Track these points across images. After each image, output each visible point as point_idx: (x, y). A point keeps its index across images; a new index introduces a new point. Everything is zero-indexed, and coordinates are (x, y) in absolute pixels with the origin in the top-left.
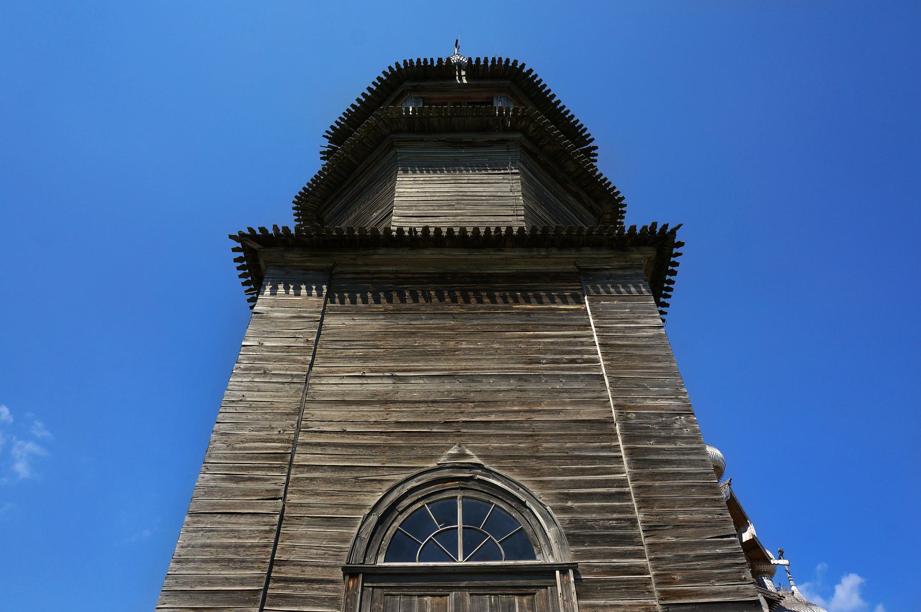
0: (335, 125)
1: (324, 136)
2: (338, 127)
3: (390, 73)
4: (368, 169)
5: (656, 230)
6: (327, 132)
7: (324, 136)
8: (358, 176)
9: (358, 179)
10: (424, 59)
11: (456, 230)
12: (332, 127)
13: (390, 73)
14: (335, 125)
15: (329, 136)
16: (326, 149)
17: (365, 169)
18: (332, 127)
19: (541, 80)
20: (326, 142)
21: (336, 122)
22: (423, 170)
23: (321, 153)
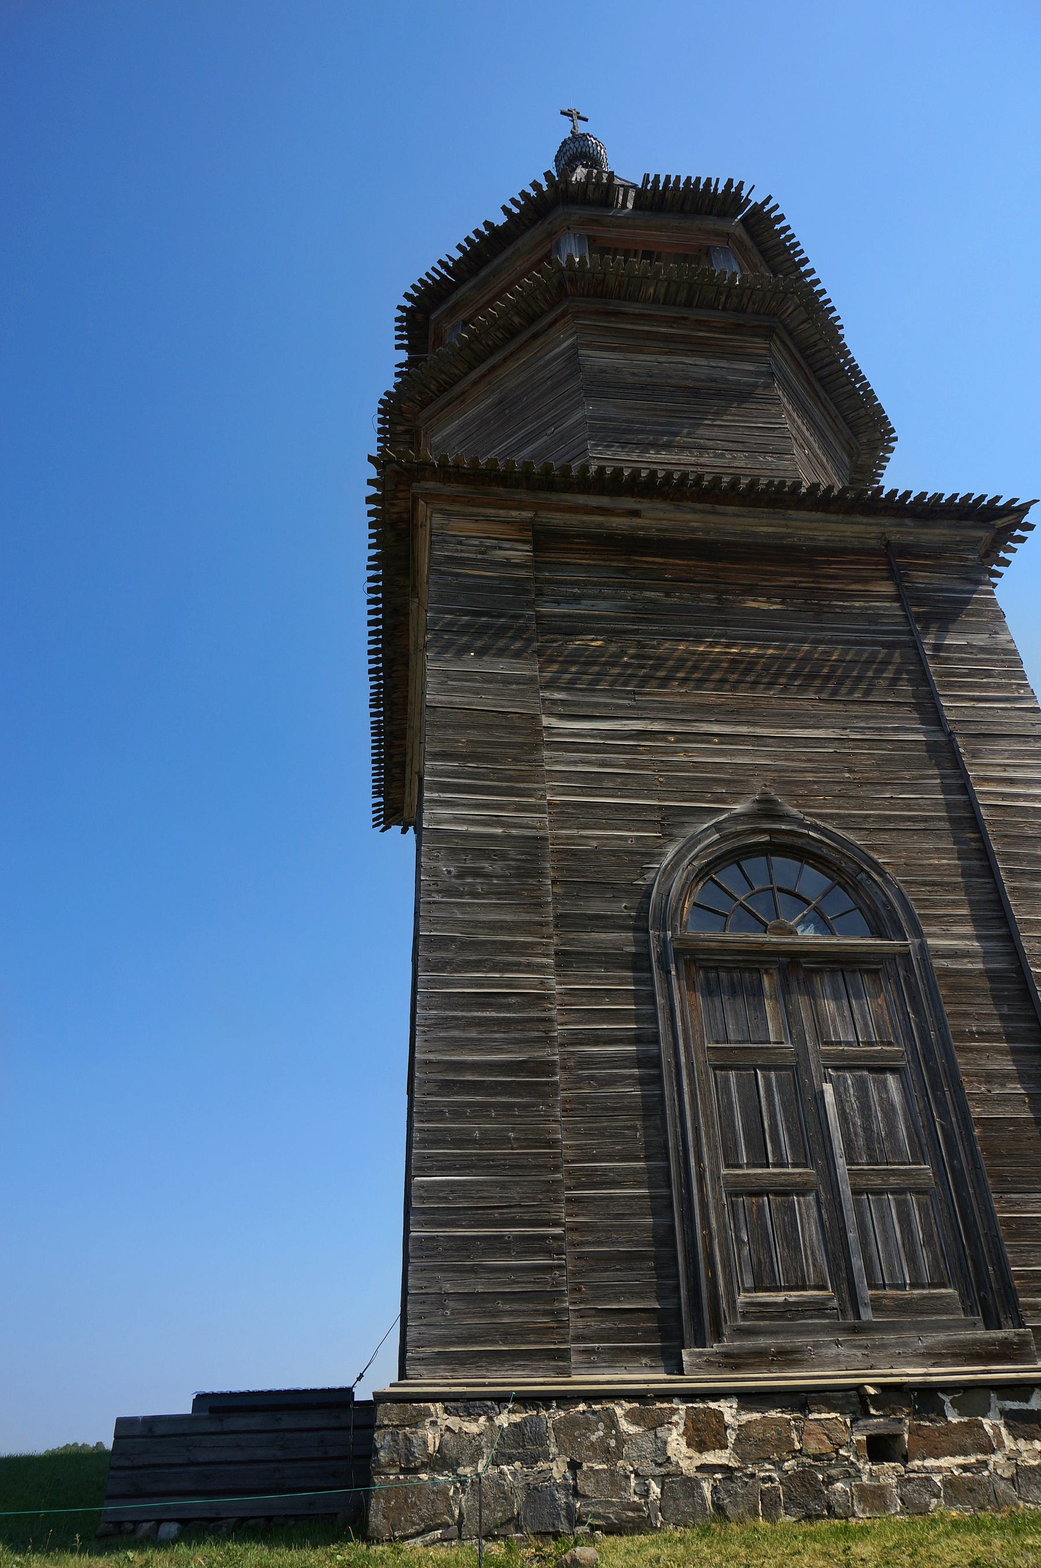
0: (783, 224)
1: (770, 198)
2: (777, 227)
3: (405, 314)
4: (828, 418)
5: (759, 1418)
6: (777, 207)
7: (770, 198)
8: (823, 405)
9: (819, 404)
10: (677, 176)
11: (745, 481)
12: (782, 217)
13: (405, 314)
14: (783, 224)
15: (767, 208)
16: (744, 193)
17: (829, 413)
18: (782, 217)
19: (812, 271)
20: (757, 198)
21: (788, 228)
22: (453, 467)
23: (741, 183)
